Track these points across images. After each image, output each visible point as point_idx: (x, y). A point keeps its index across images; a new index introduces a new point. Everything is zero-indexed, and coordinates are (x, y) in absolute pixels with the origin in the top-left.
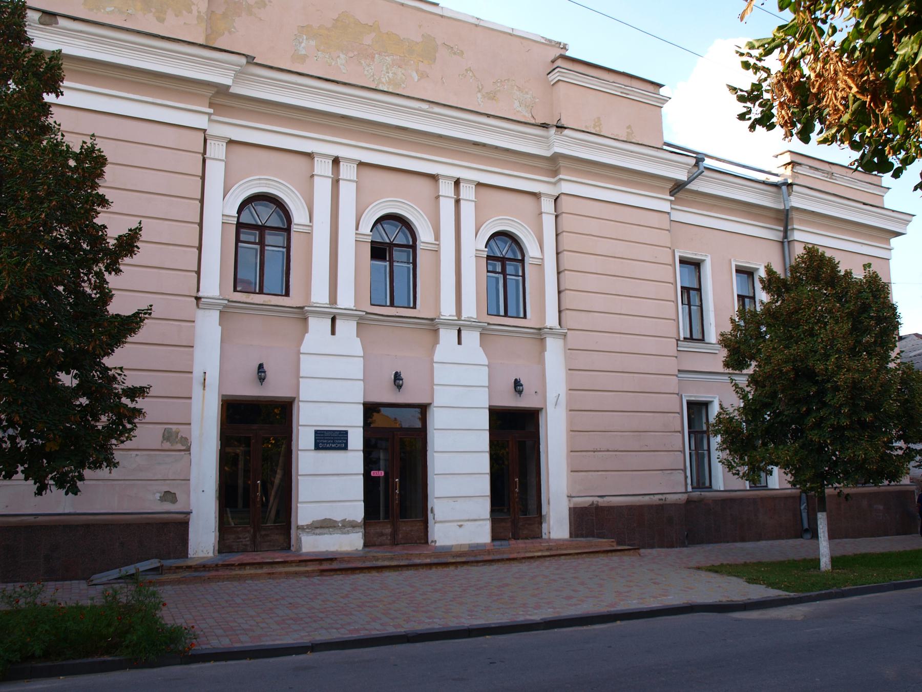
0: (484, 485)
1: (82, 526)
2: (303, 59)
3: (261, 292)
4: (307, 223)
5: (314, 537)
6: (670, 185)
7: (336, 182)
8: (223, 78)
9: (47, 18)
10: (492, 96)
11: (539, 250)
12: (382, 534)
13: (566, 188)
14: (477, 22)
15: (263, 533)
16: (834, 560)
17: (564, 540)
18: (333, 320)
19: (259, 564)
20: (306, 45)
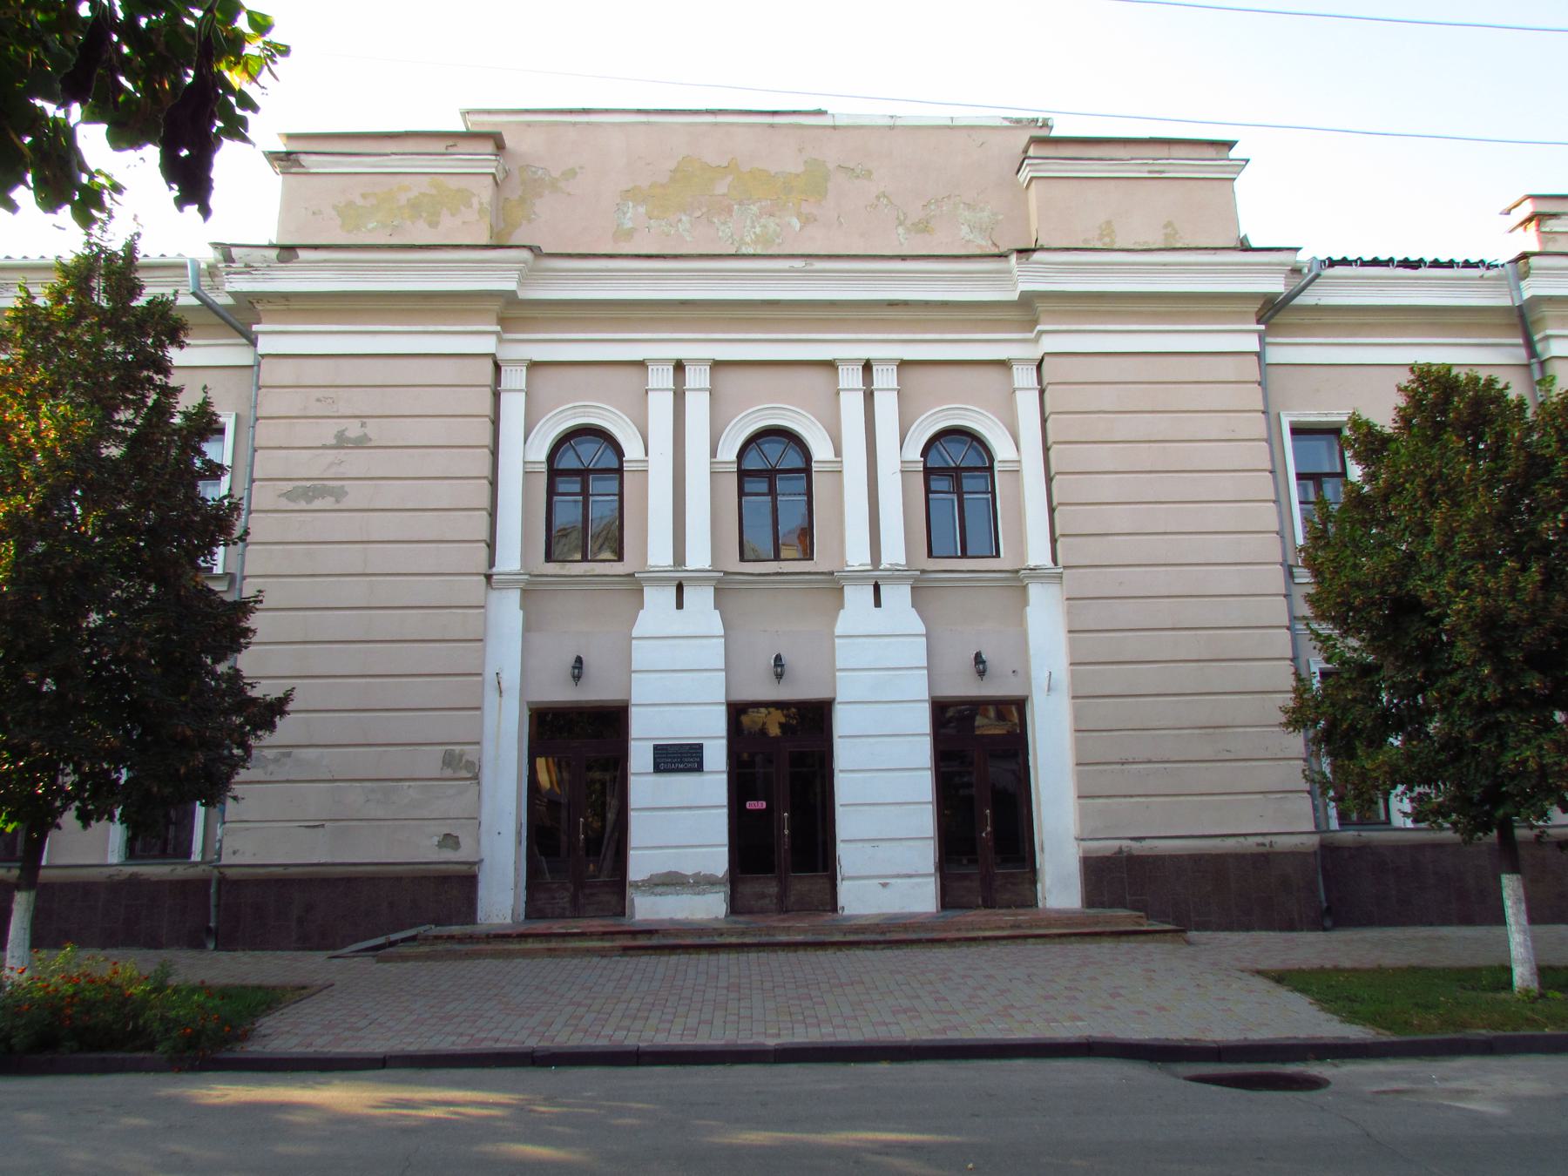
0: (926, 821)
1: (342, 879)
2: (630, 234)
3: (964, 555)
5: (653, 899)
6: (1256, 306)
7: (869, 396)
8: (506, 283)
9: (286, 254)
10: (923, 227)
11: (1015, 447)
12: (763, 896)
13: (1050, 344)
15: (587, 891)
16: (1545, 973)
17: (1074, 912)
18: (680, 588)
19: (545, 935)
20: (633, 214)
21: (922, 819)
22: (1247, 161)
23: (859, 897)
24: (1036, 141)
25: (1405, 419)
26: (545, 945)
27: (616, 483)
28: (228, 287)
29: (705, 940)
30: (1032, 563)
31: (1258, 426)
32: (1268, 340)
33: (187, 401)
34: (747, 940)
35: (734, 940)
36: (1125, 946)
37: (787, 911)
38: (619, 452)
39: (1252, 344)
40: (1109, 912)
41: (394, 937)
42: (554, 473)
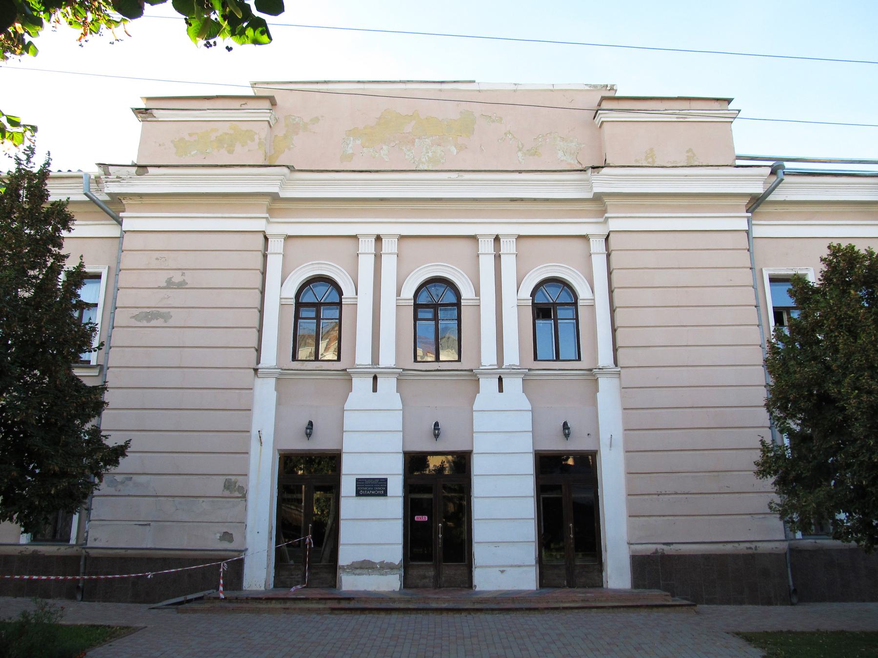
0: (529, 531)
1: (160, 559)
3: (558, 359)
4: (354, 295)
5: (353, 576)
6: (746, 201)
7: (498, 258)
9: (141, 170)
10: (534, 152)
11: (593, 293)
12: (425, 577)
13: (614, 225)
14: (515, 88)
17: (625, 591)
21: (527, 530)
22: (739, 111)
23: (486, 580)
24: (604, 98)
25: (826, 278)
26: (283, 606)
27: (338, 311)
28: (106, 190)
29: (384, 606)
30: (600, 365)
31: (747, 277)
32: (754, 222)
33: (70, 265)
34: (411, 606)
35: (402, 606)
36: (655, 614)
37: (440, 587)
38: (340, 293)
39: (743, 225)
40: (647, 592)
41: (189, 597)
42: (299, 305)
